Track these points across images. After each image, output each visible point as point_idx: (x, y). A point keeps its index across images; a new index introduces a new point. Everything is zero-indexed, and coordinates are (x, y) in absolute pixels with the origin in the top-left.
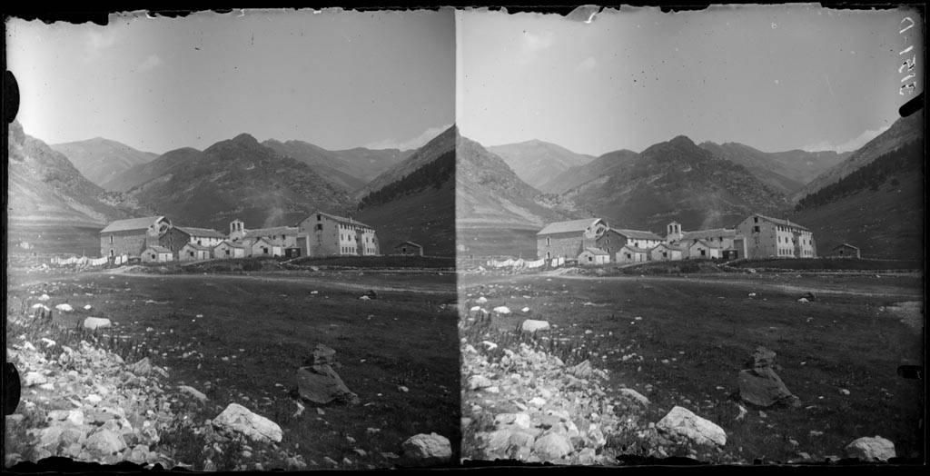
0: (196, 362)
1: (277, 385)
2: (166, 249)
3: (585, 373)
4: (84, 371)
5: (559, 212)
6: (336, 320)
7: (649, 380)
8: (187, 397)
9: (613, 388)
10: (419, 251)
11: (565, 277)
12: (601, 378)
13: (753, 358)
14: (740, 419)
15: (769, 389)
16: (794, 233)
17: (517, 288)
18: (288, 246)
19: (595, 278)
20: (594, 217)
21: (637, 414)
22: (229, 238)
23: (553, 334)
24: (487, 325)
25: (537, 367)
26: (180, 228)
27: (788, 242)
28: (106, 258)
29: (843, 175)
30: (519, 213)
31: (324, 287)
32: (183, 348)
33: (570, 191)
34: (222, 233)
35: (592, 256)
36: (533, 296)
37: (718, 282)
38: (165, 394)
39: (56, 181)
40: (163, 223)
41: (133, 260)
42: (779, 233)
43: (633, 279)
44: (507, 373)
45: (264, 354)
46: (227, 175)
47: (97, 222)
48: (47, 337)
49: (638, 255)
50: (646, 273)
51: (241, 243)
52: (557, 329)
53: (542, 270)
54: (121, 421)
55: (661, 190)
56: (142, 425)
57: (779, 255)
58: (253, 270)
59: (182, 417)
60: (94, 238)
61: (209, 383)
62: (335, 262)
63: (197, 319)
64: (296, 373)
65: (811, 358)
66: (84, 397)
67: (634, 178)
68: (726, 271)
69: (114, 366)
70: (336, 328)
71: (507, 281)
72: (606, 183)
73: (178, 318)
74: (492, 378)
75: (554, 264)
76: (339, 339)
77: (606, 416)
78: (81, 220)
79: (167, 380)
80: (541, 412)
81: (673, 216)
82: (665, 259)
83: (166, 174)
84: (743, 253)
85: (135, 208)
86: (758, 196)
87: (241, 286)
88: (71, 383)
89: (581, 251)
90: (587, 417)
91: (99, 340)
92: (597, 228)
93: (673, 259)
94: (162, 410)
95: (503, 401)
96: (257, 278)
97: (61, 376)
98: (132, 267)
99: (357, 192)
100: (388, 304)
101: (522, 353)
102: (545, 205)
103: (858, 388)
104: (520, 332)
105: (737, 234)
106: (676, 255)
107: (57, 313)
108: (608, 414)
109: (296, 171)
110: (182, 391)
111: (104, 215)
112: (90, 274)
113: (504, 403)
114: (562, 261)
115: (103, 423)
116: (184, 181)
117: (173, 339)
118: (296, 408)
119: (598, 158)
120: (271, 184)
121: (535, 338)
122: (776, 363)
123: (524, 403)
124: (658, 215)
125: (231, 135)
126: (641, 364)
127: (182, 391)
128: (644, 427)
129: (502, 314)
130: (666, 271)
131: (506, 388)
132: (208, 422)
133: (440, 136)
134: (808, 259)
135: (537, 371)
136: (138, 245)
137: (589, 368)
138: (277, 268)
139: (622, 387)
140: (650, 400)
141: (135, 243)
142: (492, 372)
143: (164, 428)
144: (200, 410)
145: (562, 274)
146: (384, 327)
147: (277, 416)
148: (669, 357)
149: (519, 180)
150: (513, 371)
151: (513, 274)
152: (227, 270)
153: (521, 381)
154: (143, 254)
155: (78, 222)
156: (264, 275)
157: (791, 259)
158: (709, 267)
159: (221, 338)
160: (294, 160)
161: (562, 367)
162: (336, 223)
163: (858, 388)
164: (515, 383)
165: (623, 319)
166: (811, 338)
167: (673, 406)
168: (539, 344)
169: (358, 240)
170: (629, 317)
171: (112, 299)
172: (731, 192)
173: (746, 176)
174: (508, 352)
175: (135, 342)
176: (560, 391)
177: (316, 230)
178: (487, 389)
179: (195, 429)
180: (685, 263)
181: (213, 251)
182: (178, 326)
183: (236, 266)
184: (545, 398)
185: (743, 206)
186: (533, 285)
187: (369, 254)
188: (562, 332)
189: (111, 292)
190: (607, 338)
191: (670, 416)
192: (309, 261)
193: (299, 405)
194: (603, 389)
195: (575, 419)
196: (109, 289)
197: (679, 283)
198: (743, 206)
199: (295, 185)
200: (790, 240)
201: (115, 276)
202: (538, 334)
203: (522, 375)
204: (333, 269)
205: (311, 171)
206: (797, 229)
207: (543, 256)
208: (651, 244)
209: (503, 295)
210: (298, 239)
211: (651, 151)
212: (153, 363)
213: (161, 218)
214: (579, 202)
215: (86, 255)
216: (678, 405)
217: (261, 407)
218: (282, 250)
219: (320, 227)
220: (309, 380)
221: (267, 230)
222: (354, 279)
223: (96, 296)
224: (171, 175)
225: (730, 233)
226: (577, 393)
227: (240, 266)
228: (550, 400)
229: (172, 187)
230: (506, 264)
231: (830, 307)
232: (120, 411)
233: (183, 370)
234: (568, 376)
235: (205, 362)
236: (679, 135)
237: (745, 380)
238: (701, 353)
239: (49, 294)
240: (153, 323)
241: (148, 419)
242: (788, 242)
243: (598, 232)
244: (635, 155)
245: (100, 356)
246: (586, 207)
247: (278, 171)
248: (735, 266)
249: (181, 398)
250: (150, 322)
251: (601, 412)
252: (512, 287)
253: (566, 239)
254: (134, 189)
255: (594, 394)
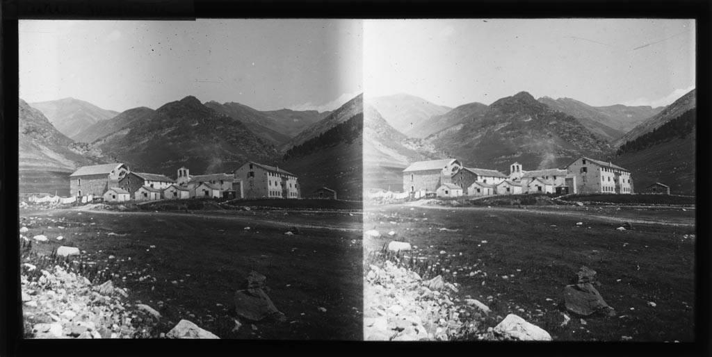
0: (481, 280)
1: (548, 299)
2: (125, 191)
3: (108, 291)
4: (388, 286)
5: (422, 153)
6: (596, 247)
7: (491, 293)
8: (473, 308)
9: (460, 299)
10: (666, 190)
11: (92, 211)
12: (121, 295)
13: (247, 280)
14: (236, 331)
15: (589, 301)
16: (282, 178)
17: (53, 220)
18: (558, 185)
19: (117, 213)
20: (118, 162)
21: (150, 325)
22: (176, 182)
23: (82, 259)
24: (28, 250)
25: (69, 285)
26: (469, 169)
27: (610, 180)
28: (75, 197)
29: (657, 126)
30: (56, 159)
31: (588, 219)
32: (470, 268)
33: (98, 140)
34: (504, 173)
35: (115, 194)
36: (66, 227)
37: (551, 213)
38: (455, 306)
39: (34, 133)
40: (122, 169)
41: (97, 199)
42: (603, 173)
43: (149, 214)
44: (44, 290)
45: (537, 274)
46: (509, 125)
47: (400, 163)
48: (28, 262)
49: (153, 194)
50: (492, 205)
51: (519, 181)
52: (86, 254)
53: (74, 206)
54: (418, 328)
55: (173, 141)
56: (435, 331)
57: (269, 196)
58: (529, 205)
59: (469, 324)
60: (65, 181)
61: (491, 297)
62: (596, 199)
63: (151, 249)
64: (564, 290)
65: (625, 276)
66: (61, 313)
67: (151, 130)
68: (226, 209)
69: (83, 287)
70: (597, 253)
71: (45, 214)
72: (127, 135)
73: (135, 248)
74: (31, 294)
75: (84, 200)
76: (599, 262)
77: (453, 321)
78: (388, 161)
79: (457, 294)
80: (71, 323)
81: (516, 158)
82: (508, 193)
83: (458, 124)
84: (573, 189)
85: (99, 156)
86: (253, 147)
87: (518, 218)
88: (50, 301)
89: (106, 190)
90: (109, 328)
91: (401, 260)
92: (453, 167)
93: (182, 198)
94: (125, 324)
95: (40, 313)
96: (532, 211)
97: (41, 294)
98: (429, 201)
99: (615, 141)
100: (640, 234)
101: (56, 273)
102: (77, 152)
103: (663, 301)
104: (55, 256)
105: (568, 173)
106: (184, 195)
107: (35, 243)
108: (127, 325)
109: (566, 123)
110: (469, 303)
111: (73, 162)
112: (394, 206)
113: (41, 315)
114: (90, 198)
115: (403, 329)
116: (472, 130)
117: (462, 260)
118: (563, 319)
119: (454, 110)
120: (212, 138)
121: (67, 262)
122: (597, 280)
123: (58, 315)
124: (503, 157)
125: (512, 92)
126: (485, 279)
127: (469, 303)
128: (484, 331)
129: (40, 241)
130: (176, 208)
131: (43, 302)
132: (490, 329)
133: (686, 95)
134: (294, 199)
135: (69, 289)
136: (435, 182)
137: (111, 287)
138: (549, 203)
139: (138, 303)
140: (490, 309)
141: (431, 180)
142: (31, 289)
143: (454, 334)
144: (483, 319)
145: (90, 209)
146: (636, 253)
147: (547, 324)
148: (178, 279)
149: (56, 130)
150: (49, 288)
151: (50, 208)
152: (174, 209)
153: (55, 297)
154: (438, 190)
155: (52, 168)
156: (538, 209)
157: (279, 199)
158: (545, 200)
159: (502, 261)
160: (231, 118)
161: (89, 286)
162: (598, 167)
163: (663, 301)
164: (50, 298)
165: (471, 242)
166: (626, 260)
167: (181, 319)
168: (70, 267)
169: (616, 180)
170: (477, 240)
171: (412, 227)
172: (564, 138)
173: (243, 131)
174: (45, 272)
175: (431, 263)
176: (88, 305)
177: (581, 172)
178: (27, 303)
179: (479, 335)
180: (525, 196)
181: (163, 193)
182: (136, 255)
183: (515, 201)
184: (75, 311)
185: (240, 155)
186: (398, 213)
187: (625, 193)
188: (90, 257)
189: (79, 225)
190: (458, 258)
191: (504, 322)
192: (576, 197)
193: (566, 316)
194: (122, 304)
195: (99, 329)
196: (410, 218)
197: (187, 217)
198: (240, 155)
199: (565, 135)
200: (612, 179)
201: (415, 207)
202: (70, 258)
203: (56, 292)
204: (595, 204)
205: (577, 124)
206: (285, 174)
207: (75, 194)
208: (164, 185)
209: (42, 225)
210: (566, 180)
211: (164, 108)
212: (115, 285)
213: (454, 160)
214: (105, 150)
215: (391, 190)
216: (185, 319)
217: (535, 318)
218: (220, 193)
219: (585, 169)
220: (575, 295)
221: (540, 171)
222: (612, 214)
223: (398, 224)
224: (129, 130)
225: (229, 177)
226: (102, 307)
227: (518, 201)
228: (79, 313)
229: (463, 135)
230: (44, 200)
231: (642, 235)
232: (417, 320)
233: (469, 285)
234: (94, 293)
235: (488, 280)
236: (188, 95)
237: (240, 299)
238: (204, 276)
239: (28, 227)
240: (114, 252)
241: (440, 326)
242: (610, 180)
243: (120, 175)
244: (485, 107)
245: (401, 274)
246: (111, 154)
247: (551, 123)
248: (566, 200)
249: (468, 309)
250: (444, 246)
251: (120, 324)
252: (49, 219)
253: (94, 180)
254: (431, 136)
255: (115, 309)
